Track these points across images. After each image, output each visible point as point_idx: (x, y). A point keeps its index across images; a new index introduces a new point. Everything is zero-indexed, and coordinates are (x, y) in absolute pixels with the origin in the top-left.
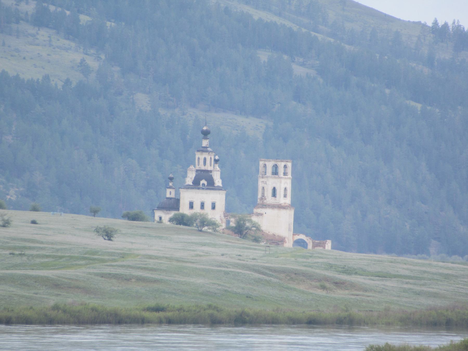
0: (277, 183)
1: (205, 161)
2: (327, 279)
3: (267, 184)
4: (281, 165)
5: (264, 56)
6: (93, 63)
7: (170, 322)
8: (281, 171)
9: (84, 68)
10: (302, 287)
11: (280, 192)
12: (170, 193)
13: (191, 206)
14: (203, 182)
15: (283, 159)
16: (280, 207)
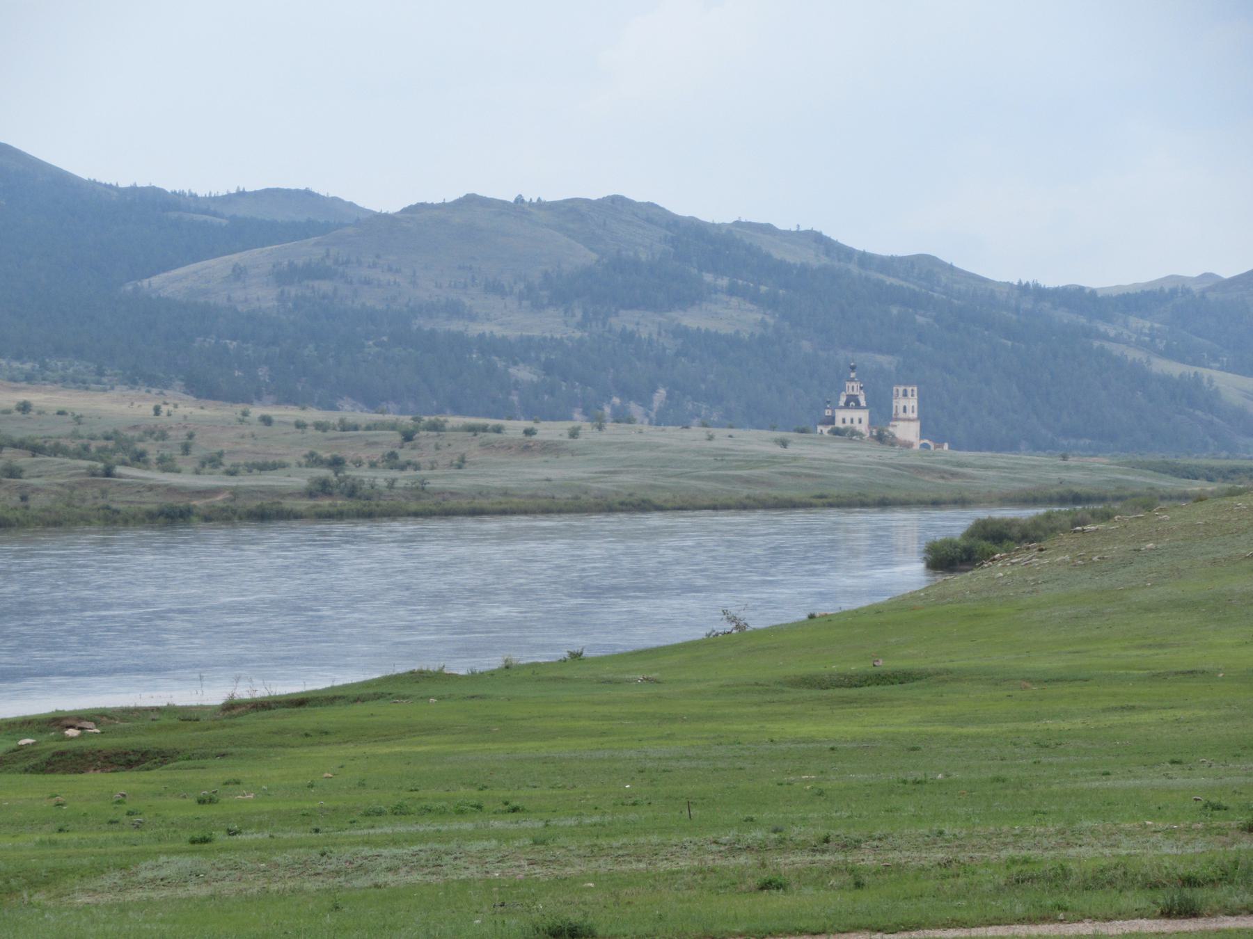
0: (907, 402)
1: (853, 388)
2: (945, 472)
3: (899, 403)
4: (909, 389)
5: (894, 310)
6: (770, 321)
7: (831, 505)
8: (909, 393)
9: (763, 324)
11: (909, 410)
12: (828, 413)
13: (844, 421)
14: (852, 403)
16: (909, 420)
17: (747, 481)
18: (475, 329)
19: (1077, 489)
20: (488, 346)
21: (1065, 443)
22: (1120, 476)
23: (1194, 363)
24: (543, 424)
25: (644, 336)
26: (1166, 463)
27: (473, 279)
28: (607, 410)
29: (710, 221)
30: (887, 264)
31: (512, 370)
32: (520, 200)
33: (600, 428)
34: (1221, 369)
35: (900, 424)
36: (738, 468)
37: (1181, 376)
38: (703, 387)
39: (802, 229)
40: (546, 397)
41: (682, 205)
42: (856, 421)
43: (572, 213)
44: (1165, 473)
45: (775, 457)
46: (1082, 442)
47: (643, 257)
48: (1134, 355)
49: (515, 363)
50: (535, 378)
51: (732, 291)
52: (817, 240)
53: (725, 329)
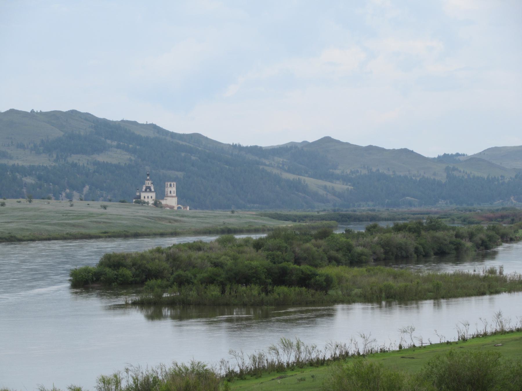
0: (172, 189)
1: (148, 183)
2: (172, 219)
3: (168, 189)
4: (172, 184)
5: (183, 154)
6: (133, 158)
7: (110, 237)
8: (172, 185)
9: (130, 160)
10: (163, 223)
11: (172, 192)
12: (138, 194)
13: (144, 197)
14: (148, 190)
15: (172, 181)
16: (172, 197)
17: (74, 225)
18: (11, 163)
19: (230, 227)
20: (15, 169)
21: (249, 206)
22: (252, 220)
23: (298, 175)
24: (8, 200)
25: (81, 164)
26: (277, 214)
27: (12, 143)
28: (64, 194)
29: (111, 120)
30: (182, 137)
31: (24, 179)
32: (32, 111)
33: (30, 201)
34: (309, 176)
35: (169, 199)
36: (73, 219)
37: (293, 179)
38: (105, 185)
39: (148, 123)
40: (38, 189)
41: (100, 114)
42: (146, 197)
43: (54, 117)
44: (274, 218)
45: (92, 214)
46: (255, 205)
47: (82, 133)
48: (275, 171)
49: (26, 176)
50: (33, 182)
51: (118, 147)
52: (154, 127)
53: (115, 162)
